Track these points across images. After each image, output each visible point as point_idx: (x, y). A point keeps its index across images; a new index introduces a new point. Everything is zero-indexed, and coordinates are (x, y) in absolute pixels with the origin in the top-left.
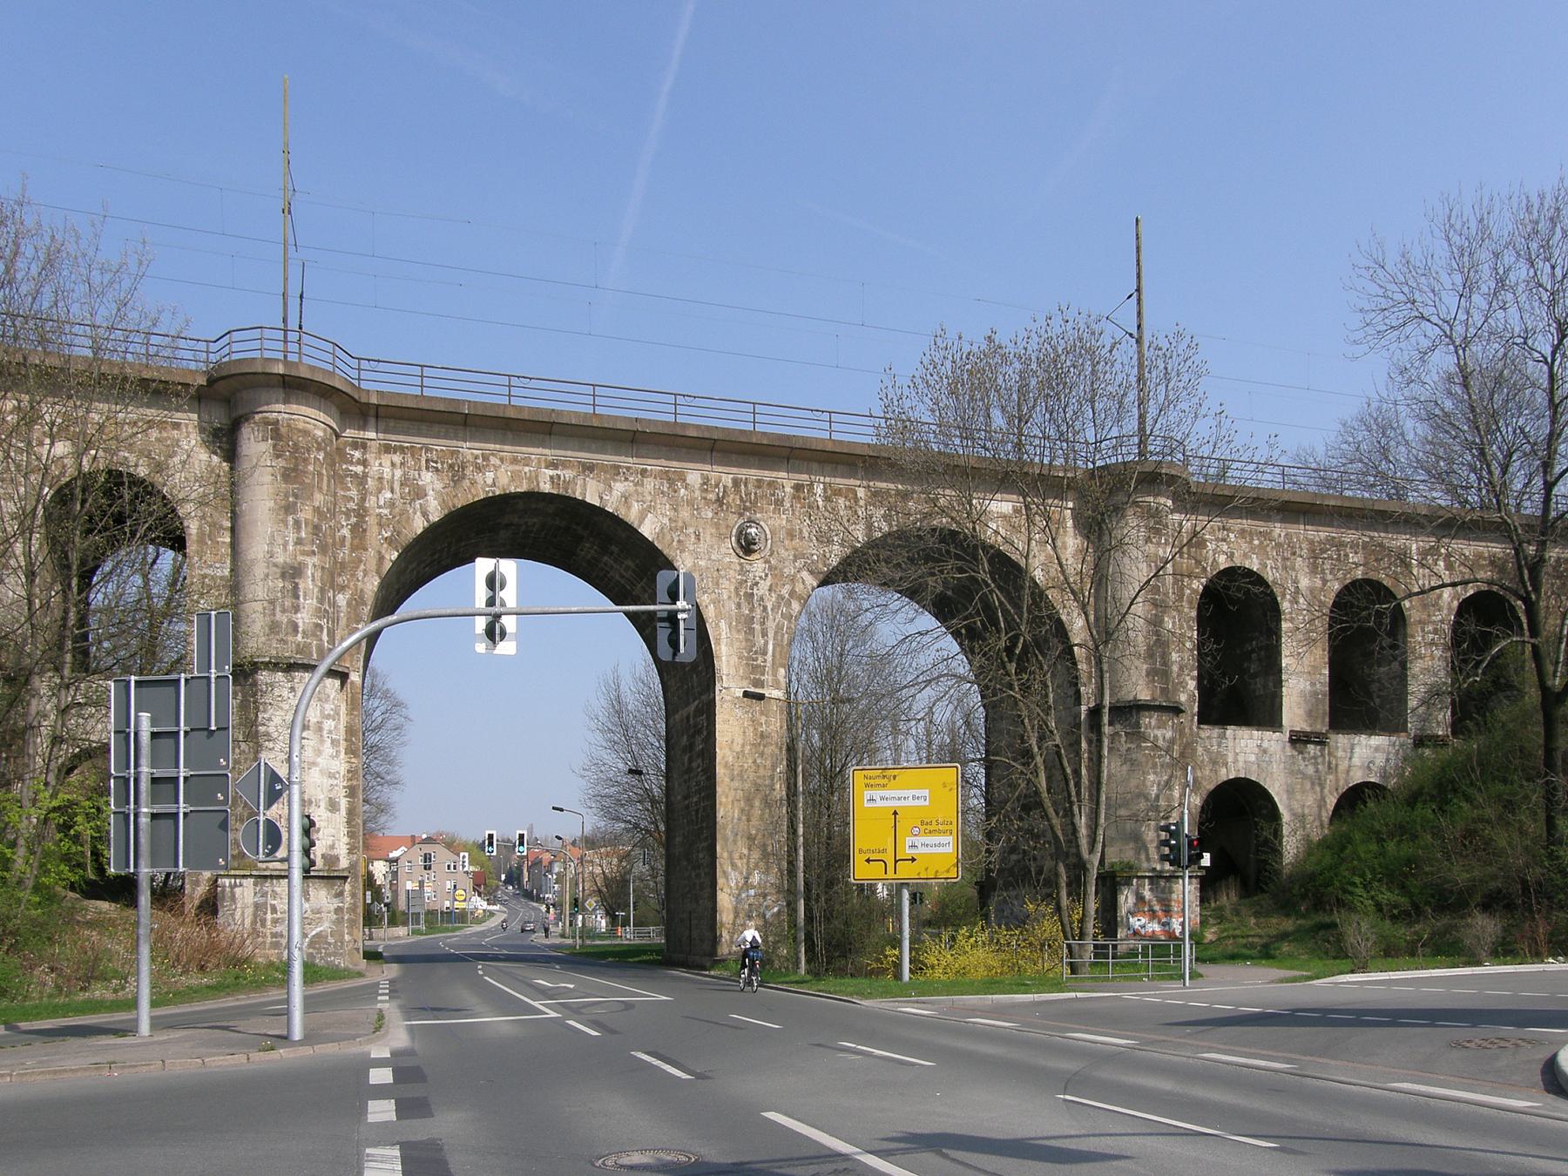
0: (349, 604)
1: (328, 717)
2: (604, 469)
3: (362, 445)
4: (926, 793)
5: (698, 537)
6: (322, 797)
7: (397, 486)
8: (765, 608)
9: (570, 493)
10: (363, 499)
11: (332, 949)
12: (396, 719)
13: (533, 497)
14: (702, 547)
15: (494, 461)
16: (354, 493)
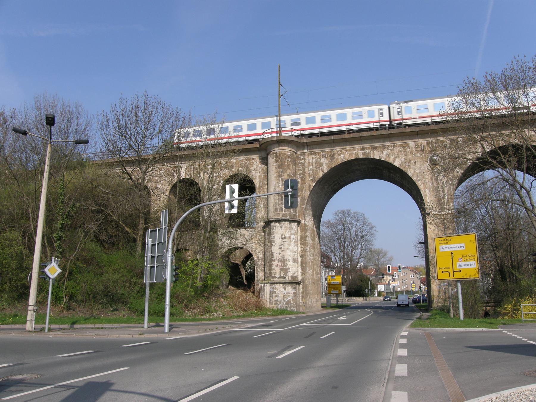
0: (301, 200)
1: (293, 234)
2: (380, 147)
3: (303, 154)
4: (463, 245)
5: (415, 163)
6: (291, 259)
7: (314, 164)
8: (443, 183)
9: (369, 157)
10: (304, 170)
11: (292, 305)
12: (372, 231)
13: (357, 160)
14: (417, 166)
15: (343, 151)
16: (301, 168)
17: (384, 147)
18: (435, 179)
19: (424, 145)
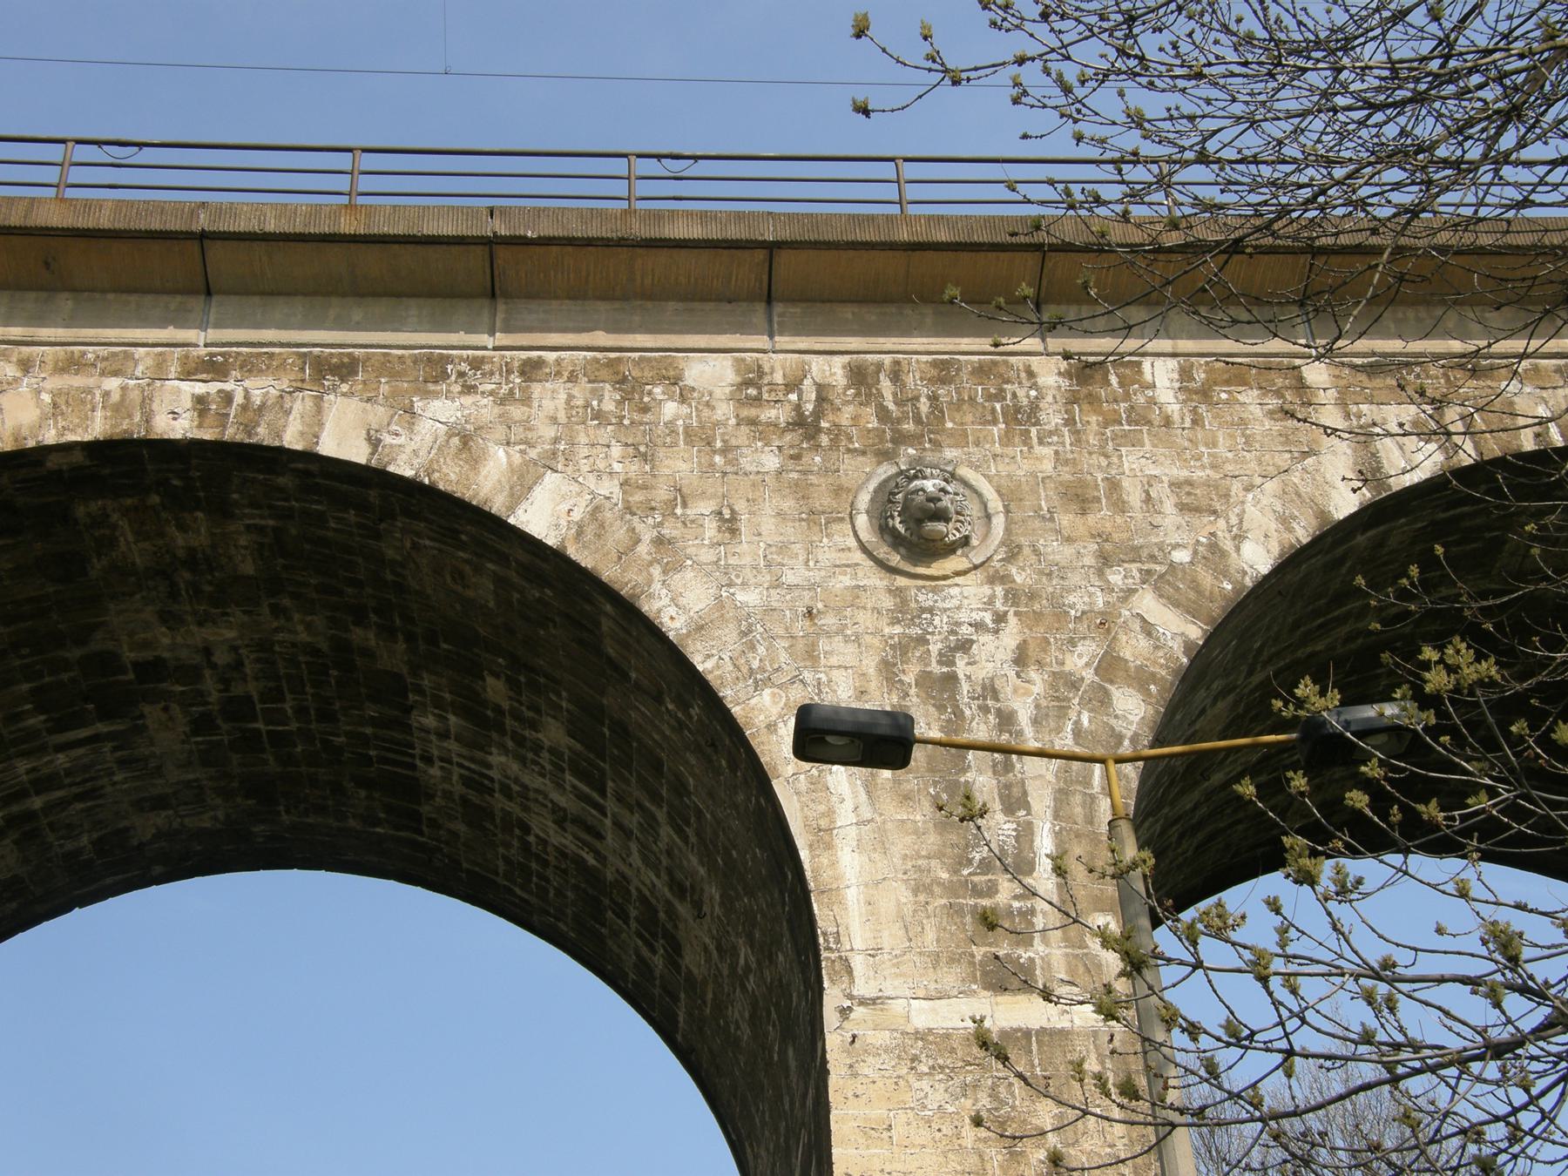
5: (729, 525)
14: (746, 551)
17: (435, 370)
18: (925, 680)
19: (822, 391)
